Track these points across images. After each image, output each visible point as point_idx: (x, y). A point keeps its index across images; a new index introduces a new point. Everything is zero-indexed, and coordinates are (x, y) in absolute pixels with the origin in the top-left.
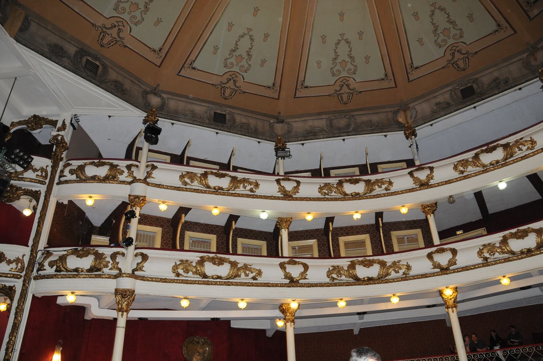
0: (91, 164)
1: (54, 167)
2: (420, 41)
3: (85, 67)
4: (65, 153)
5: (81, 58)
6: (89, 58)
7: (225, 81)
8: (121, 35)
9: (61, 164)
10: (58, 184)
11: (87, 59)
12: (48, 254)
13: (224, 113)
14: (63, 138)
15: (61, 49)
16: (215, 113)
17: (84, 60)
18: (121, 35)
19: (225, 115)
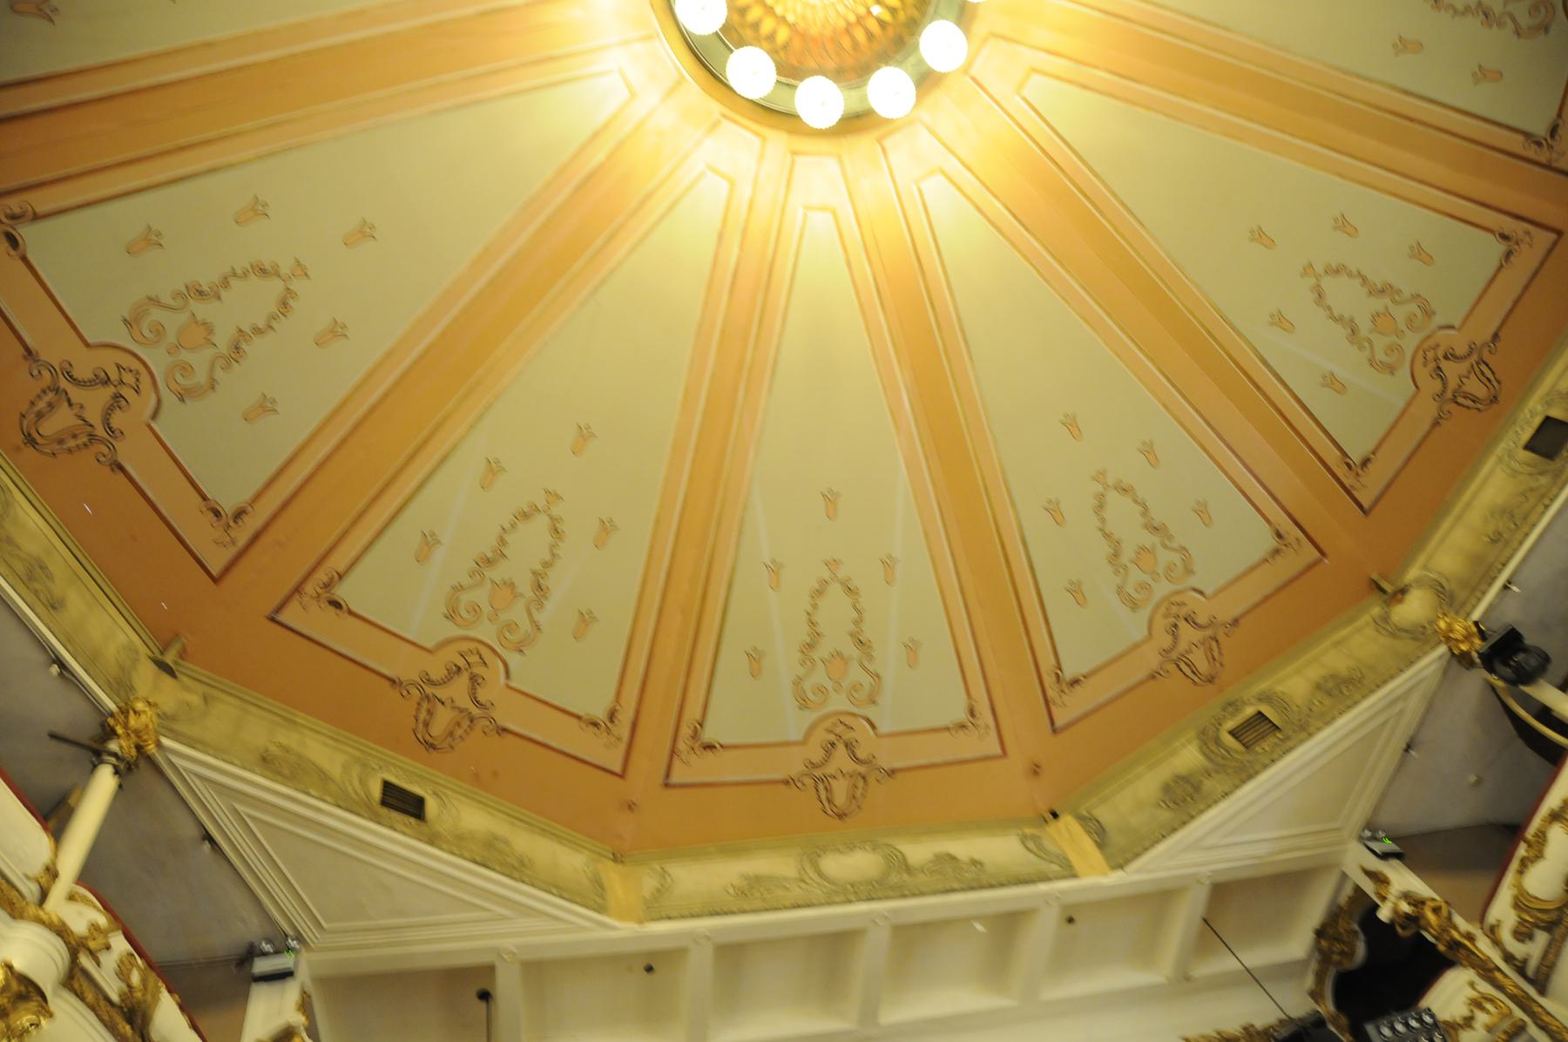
0: (1521, 872)
1: (1486, 971)
2: (1076, 591)
3: (1246, 746)
4: (1459, 920)
5: (1218, 742)
6: (1231, 724)
7: (1438, 384)
8: (117, 420)
9: (1484, 946)
10: (1542, 991)
11: (1232, 733)
12: (1492, 933)
13: (1537, 421)
14: (1406, 896)
15: (1181, 779)
16: (1529, 447)
17: (1229, 741)
18: (117, 420)
19: (1548, 419)
